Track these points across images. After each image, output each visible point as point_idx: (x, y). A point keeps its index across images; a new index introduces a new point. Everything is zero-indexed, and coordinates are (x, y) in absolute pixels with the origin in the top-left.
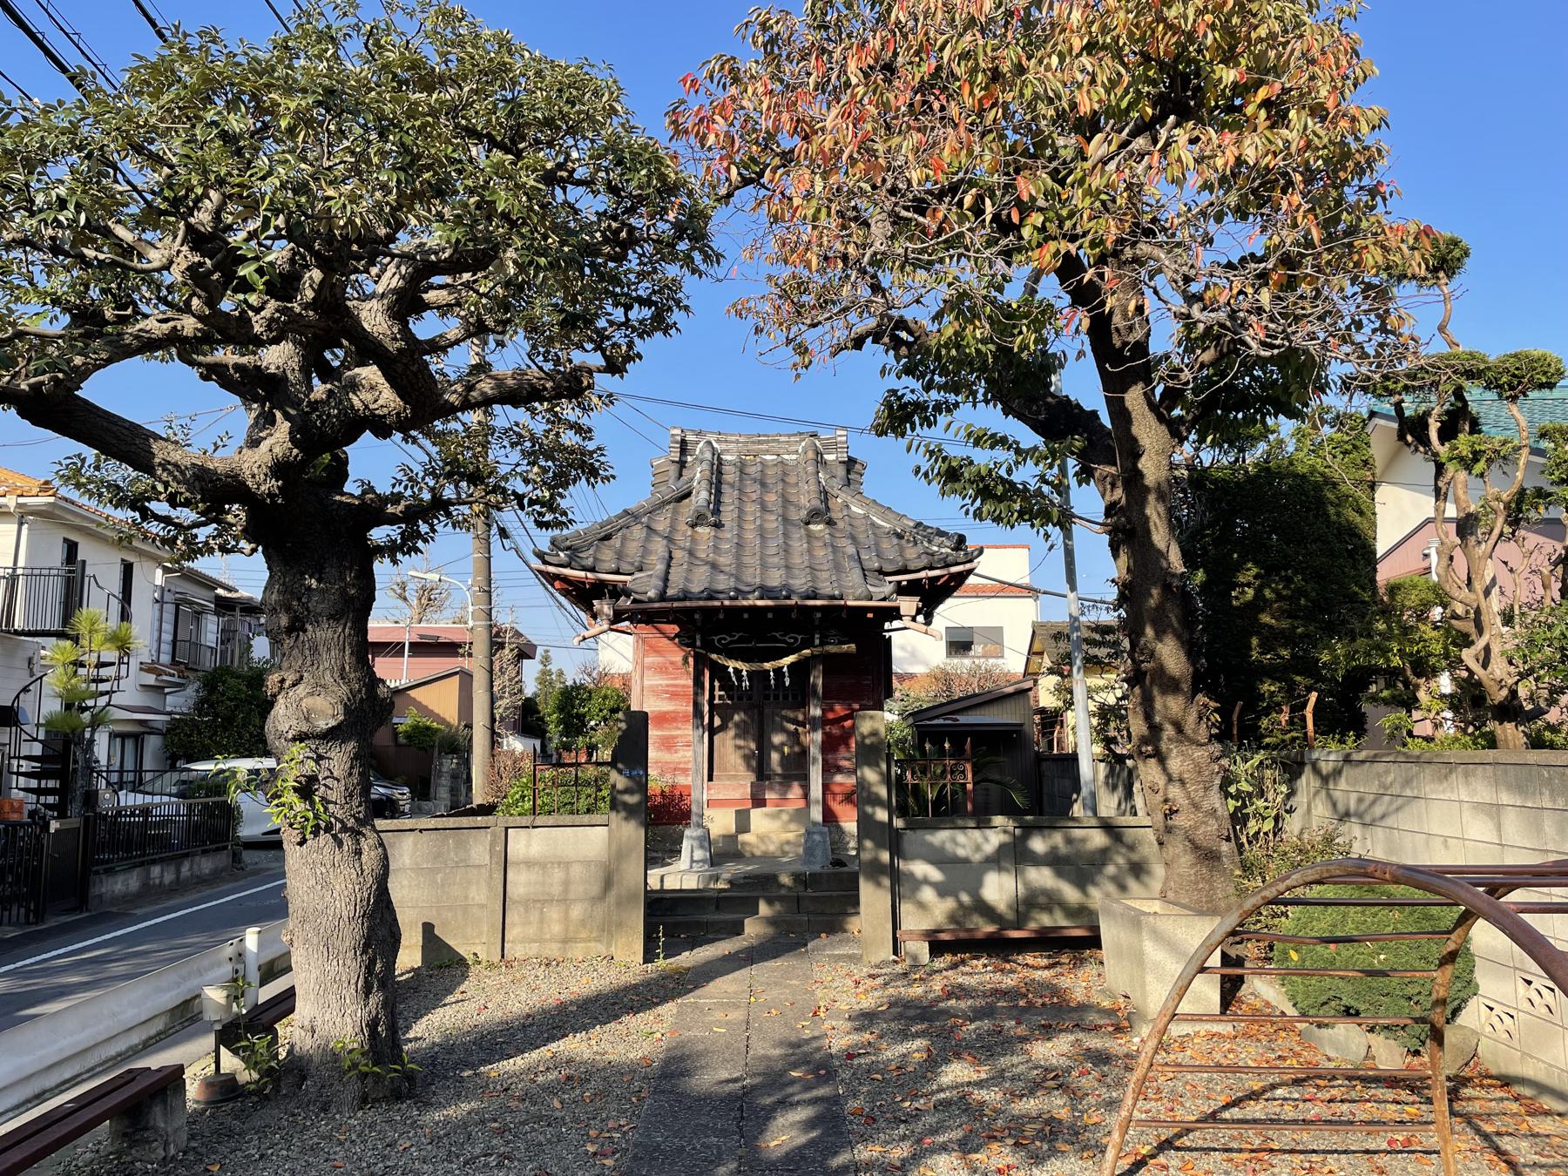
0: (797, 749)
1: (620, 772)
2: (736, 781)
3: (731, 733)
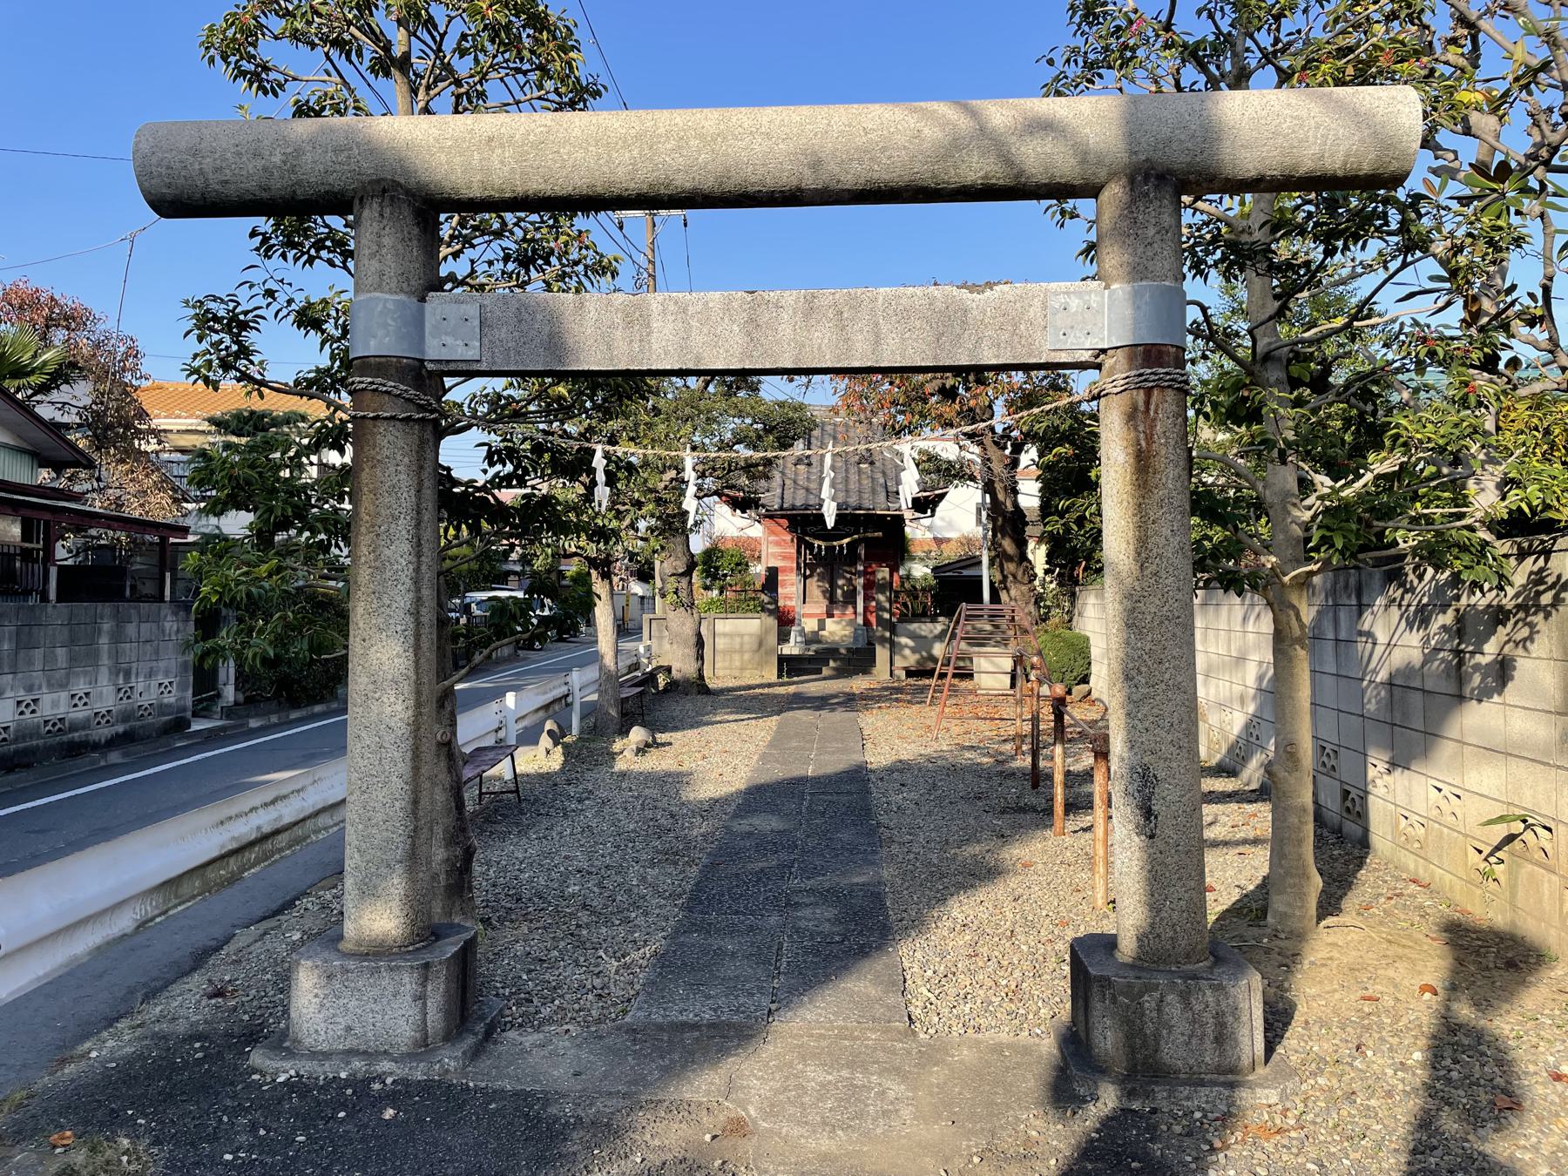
2: (818, 605)
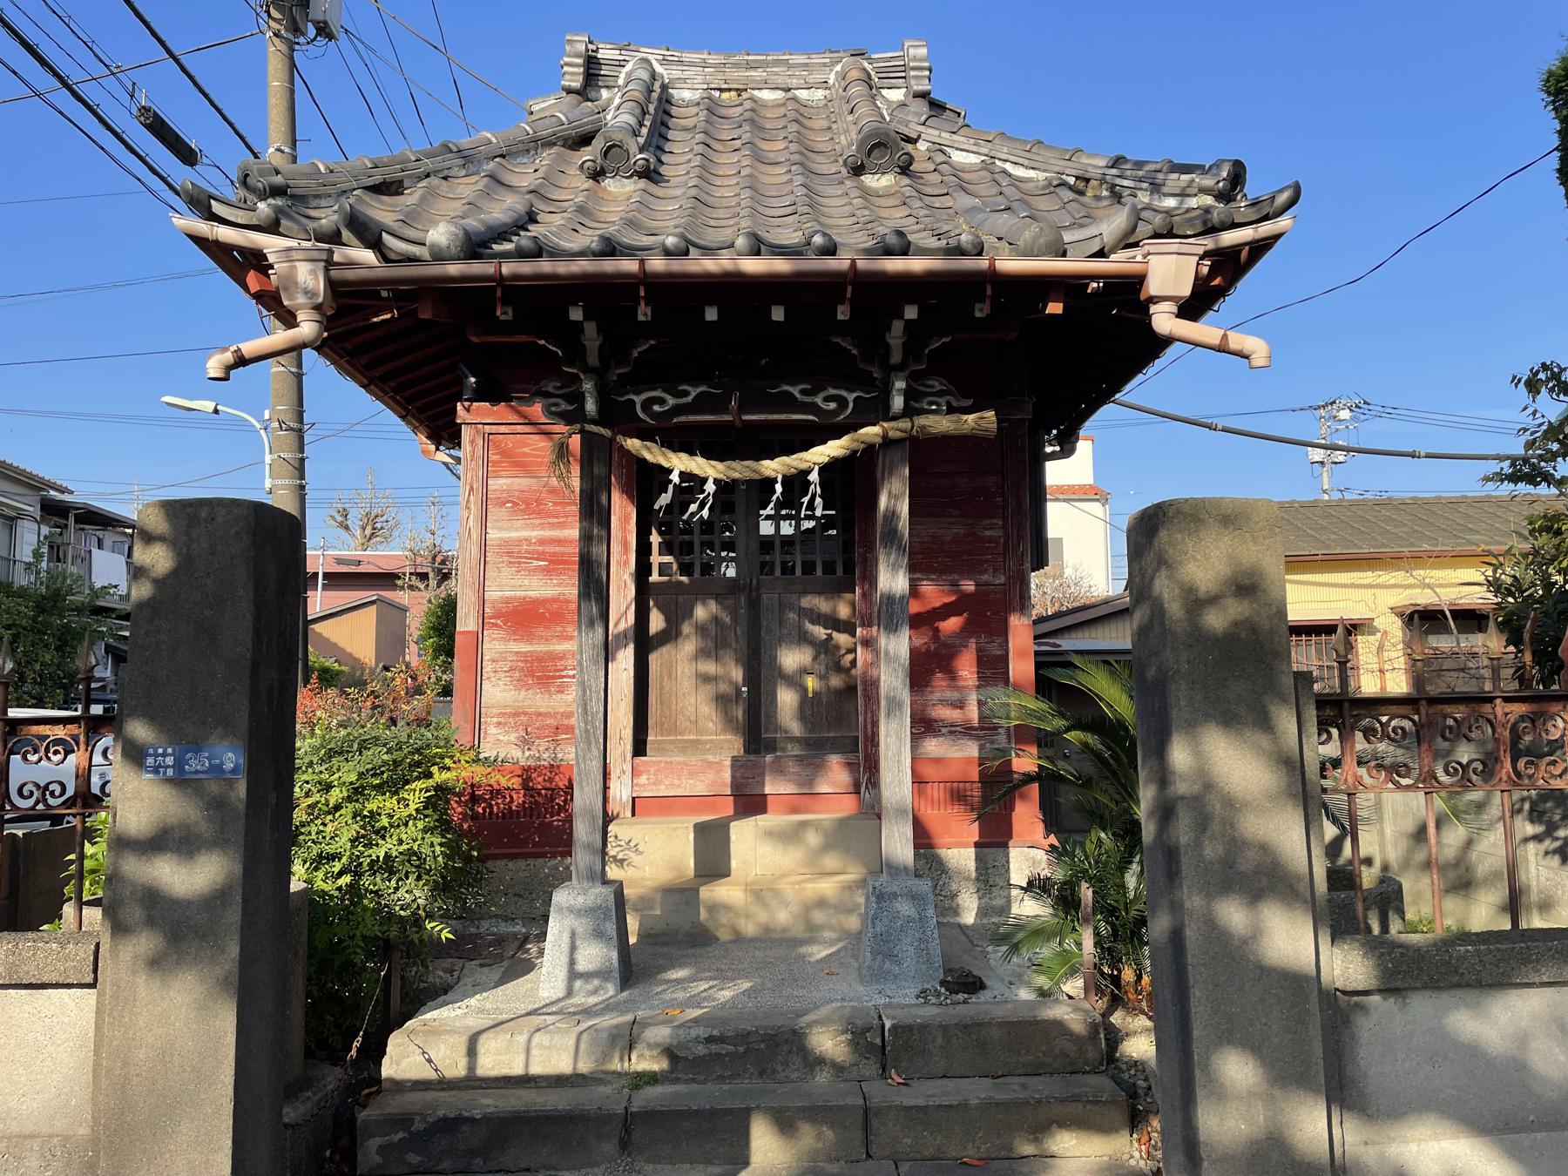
0: (836, 681)
1: (135, 754)
2: (701, 759)
3: (688, 646)
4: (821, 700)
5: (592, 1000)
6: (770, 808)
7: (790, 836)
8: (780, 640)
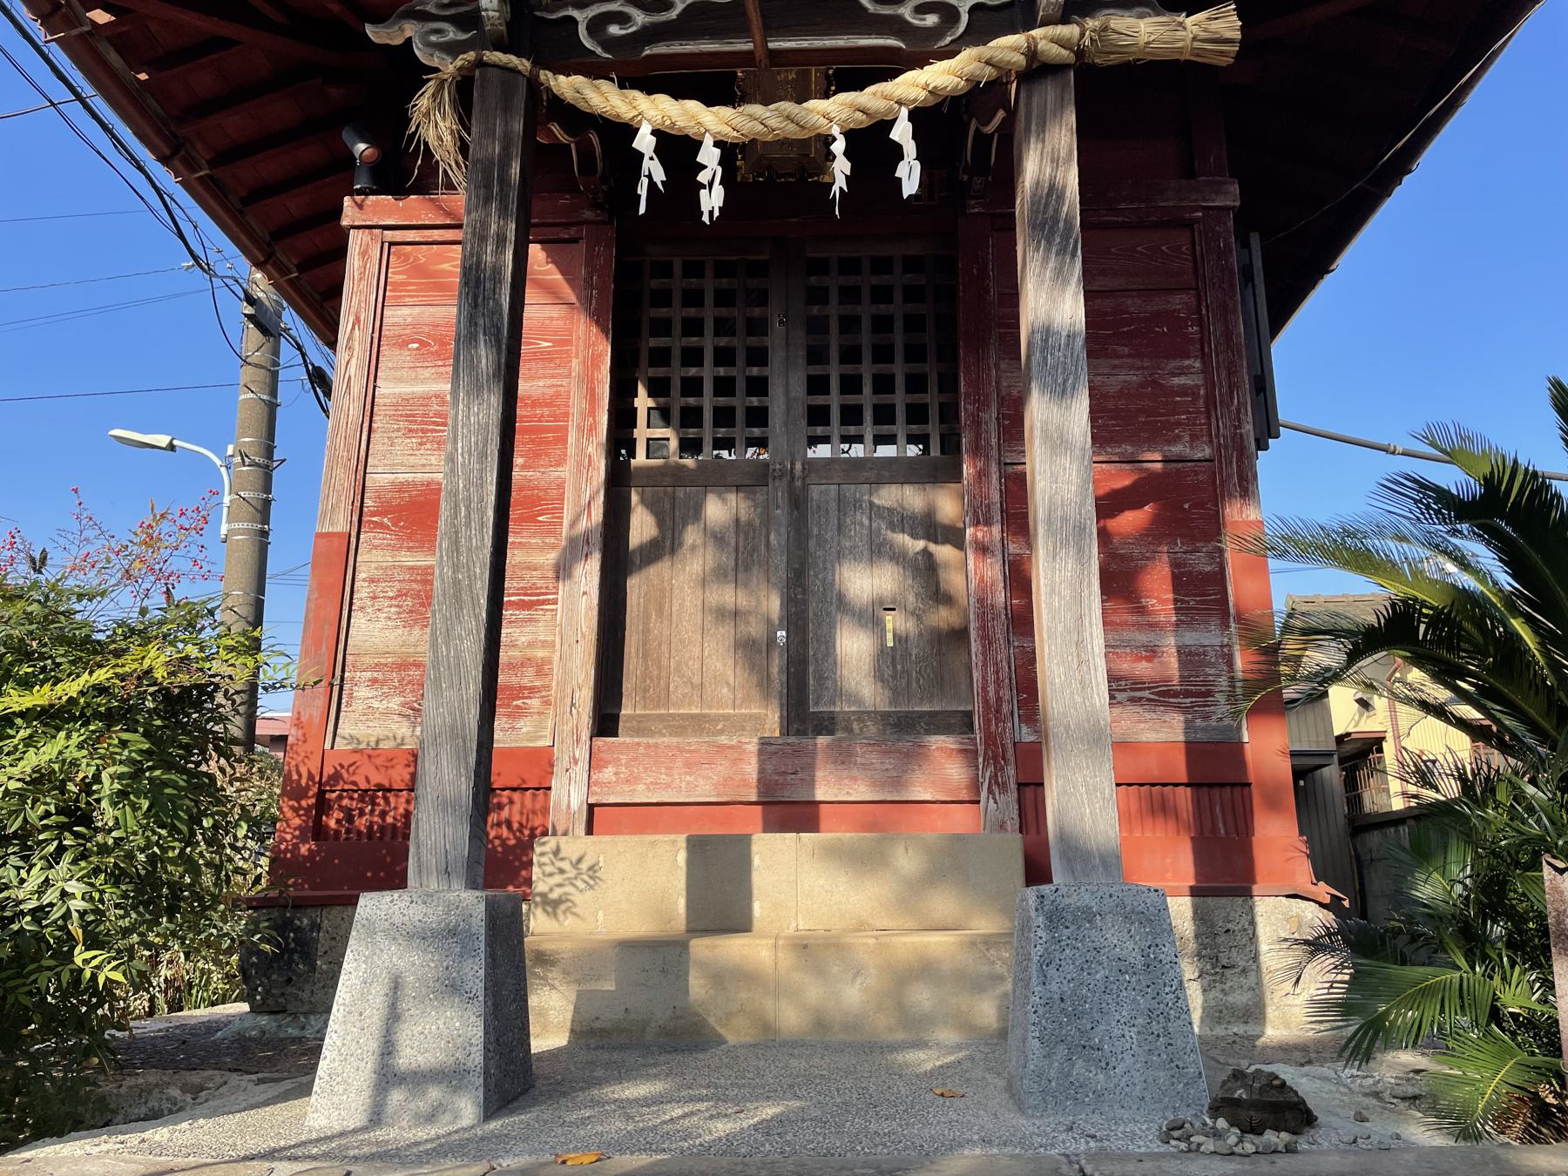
4: (906, 654)
5: (422, 1133)
6: (823, 825)
7: (864, 861)
8: (840, 556)
